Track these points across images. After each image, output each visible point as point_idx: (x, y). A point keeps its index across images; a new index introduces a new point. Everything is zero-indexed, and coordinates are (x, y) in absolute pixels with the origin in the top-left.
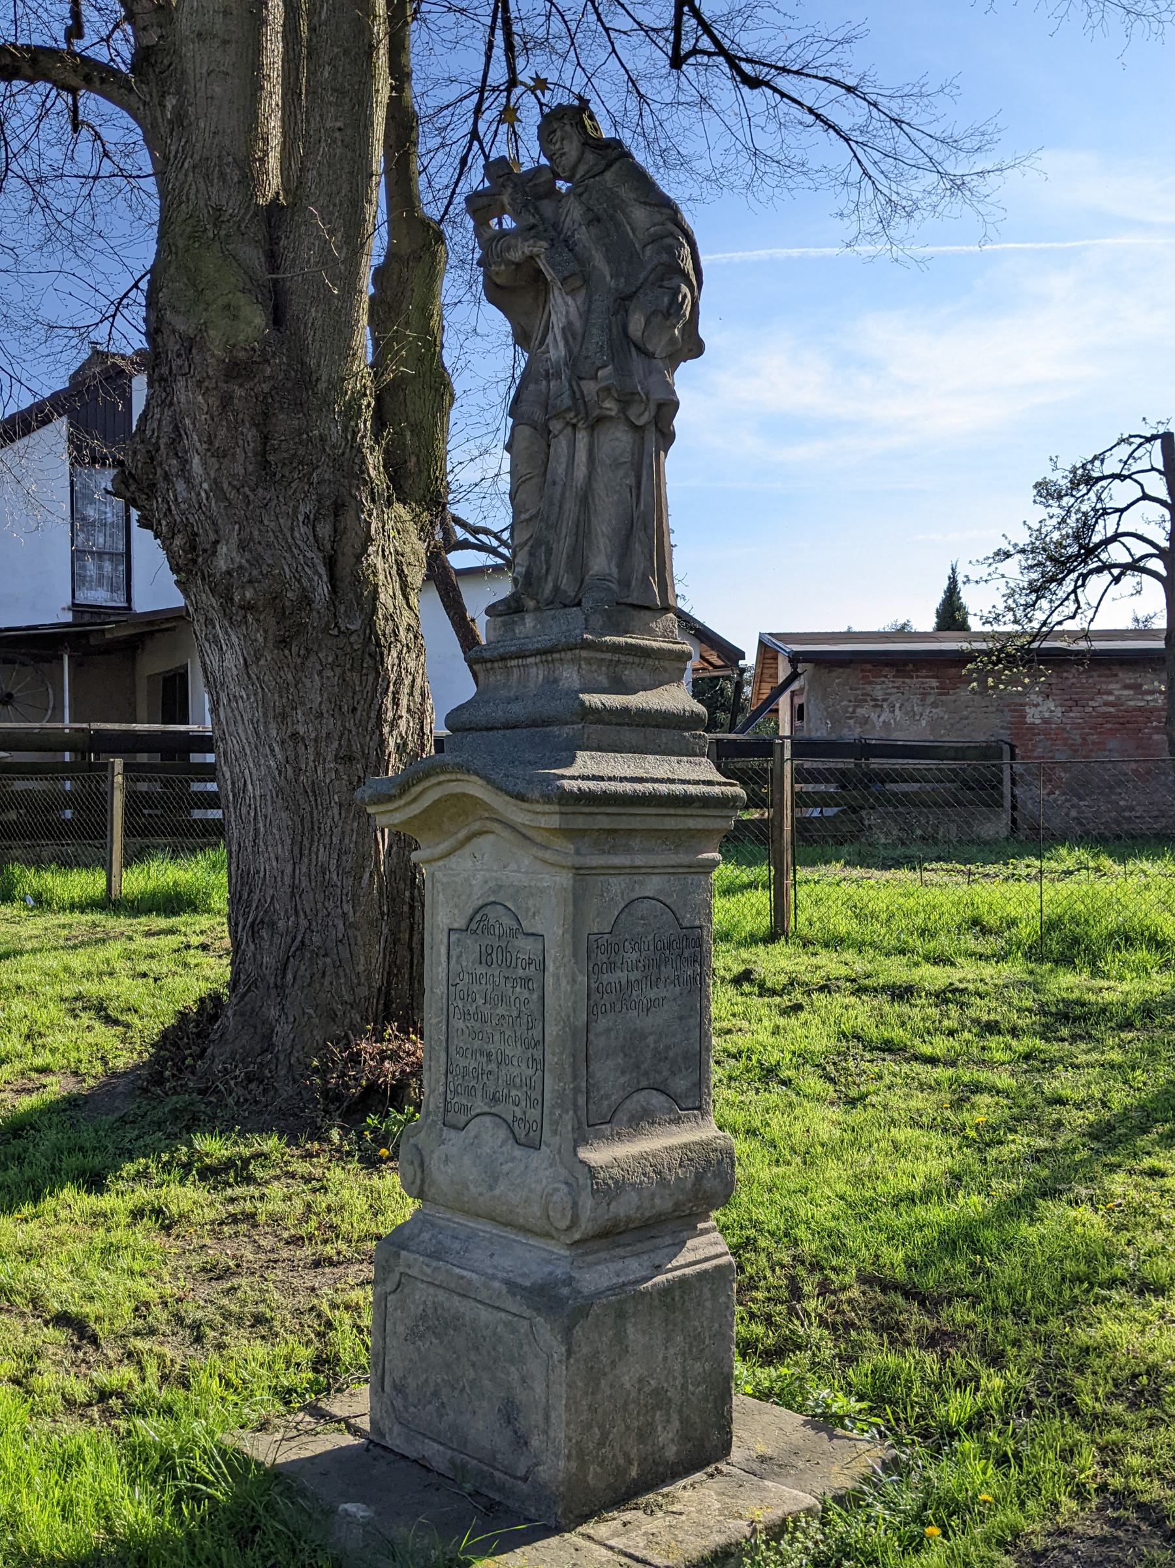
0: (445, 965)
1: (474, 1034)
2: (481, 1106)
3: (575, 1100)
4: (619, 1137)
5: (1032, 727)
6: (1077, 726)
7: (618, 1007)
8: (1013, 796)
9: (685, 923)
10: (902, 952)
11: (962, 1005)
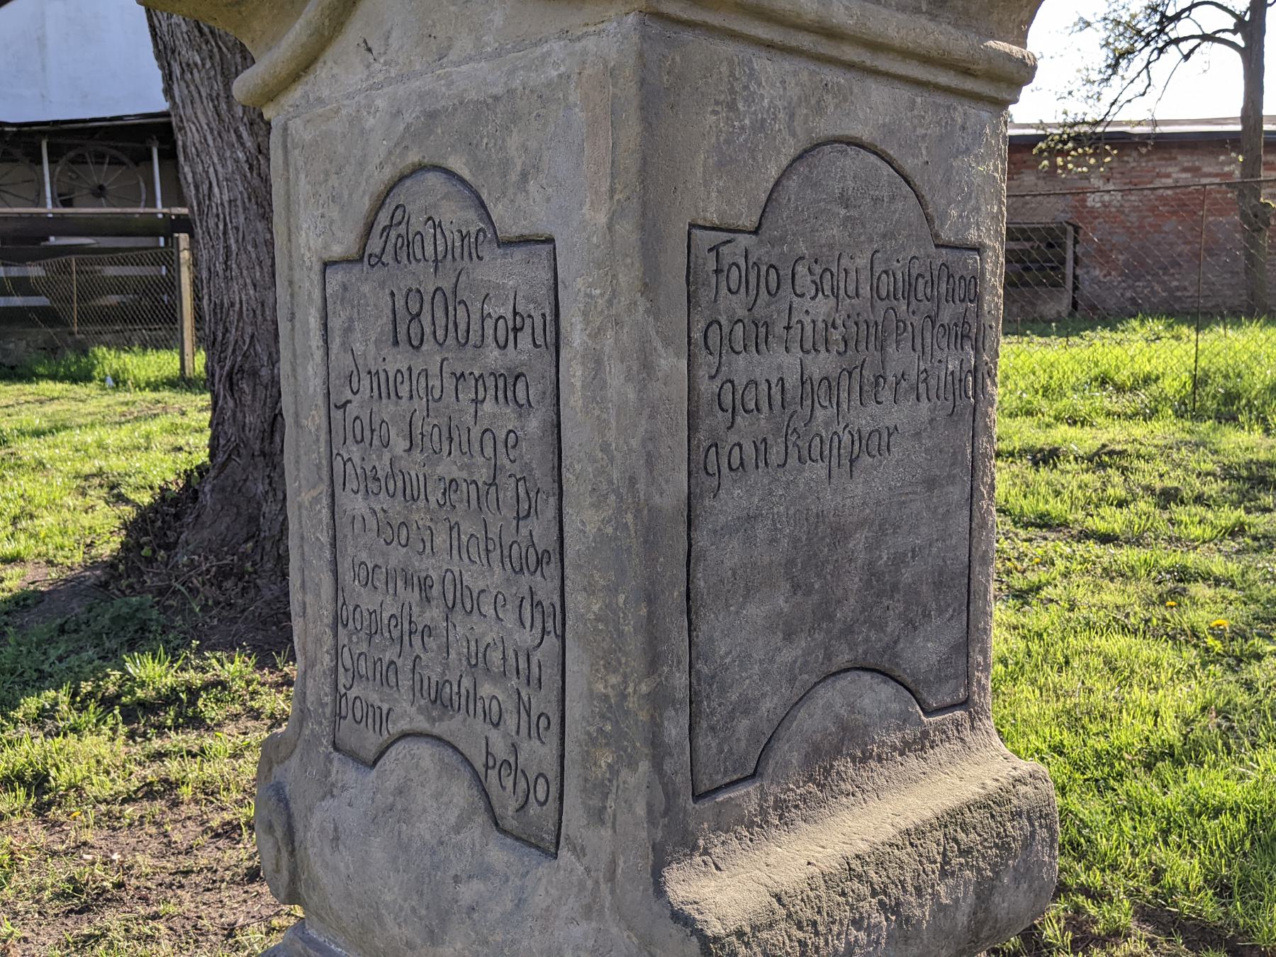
0: (318, 355)
1: (392, 530)
2: (409, 715)
3: (655, 728)
4: (782, 813)
5: (1092, 210)
6: (1136, 209)
7: (776, 455)
8: (1075, 277)
9: (947, 235)
10: (1029, 413)
11: (1124, 470)
